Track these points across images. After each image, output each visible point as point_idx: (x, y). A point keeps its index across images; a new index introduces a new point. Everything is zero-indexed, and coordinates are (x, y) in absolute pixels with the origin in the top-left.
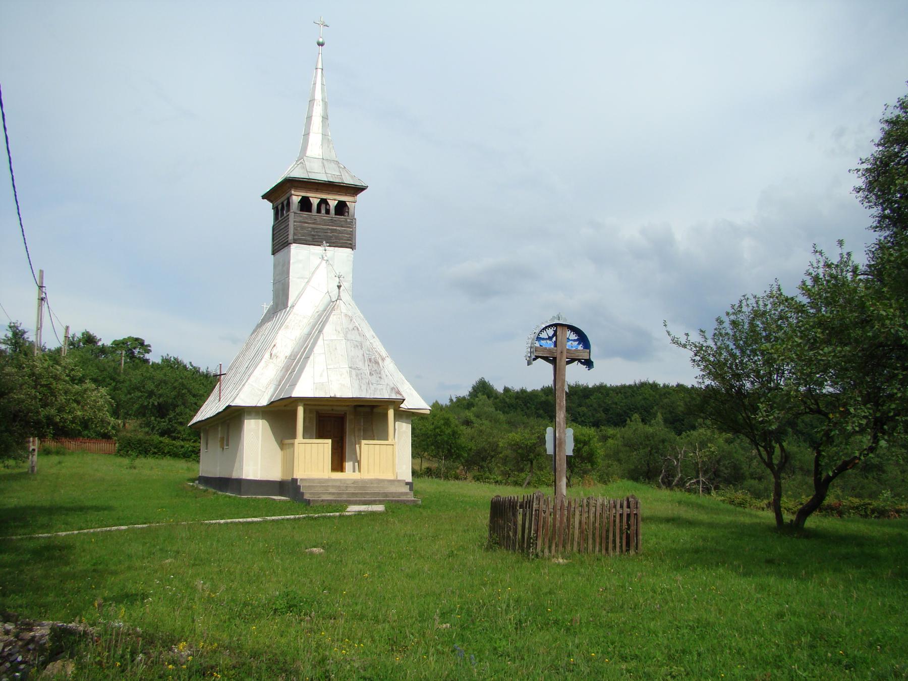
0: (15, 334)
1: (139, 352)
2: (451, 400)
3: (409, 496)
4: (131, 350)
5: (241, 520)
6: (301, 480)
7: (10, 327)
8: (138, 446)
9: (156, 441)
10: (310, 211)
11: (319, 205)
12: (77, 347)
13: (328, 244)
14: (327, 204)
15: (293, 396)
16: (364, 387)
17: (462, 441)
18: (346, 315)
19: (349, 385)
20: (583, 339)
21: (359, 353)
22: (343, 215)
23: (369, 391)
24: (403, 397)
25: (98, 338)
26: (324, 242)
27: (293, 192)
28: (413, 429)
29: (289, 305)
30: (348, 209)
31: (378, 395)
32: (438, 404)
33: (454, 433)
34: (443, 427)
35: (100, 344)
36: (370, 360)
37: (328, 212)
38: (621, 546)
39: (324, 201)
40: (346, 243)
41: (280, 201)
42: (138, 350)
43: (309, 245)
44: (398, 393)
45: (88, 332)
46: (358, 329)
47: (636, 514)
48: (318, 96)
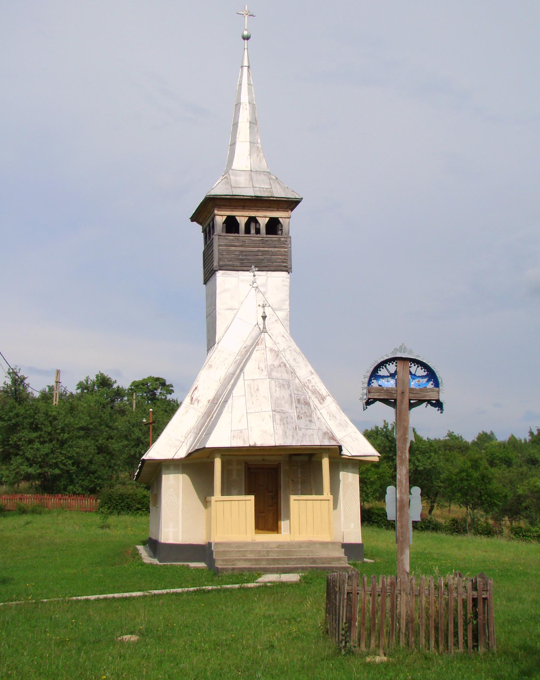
0: (15, 381)
1: (160, 393)
2: (531, 433)
3: (342, 562)
4: (152, 391)
5: (116, 595)
6: (216, 544)
7: (9, 374)
8: (120, 501)
9: (140, 496)
10: (238, 233)
11: (248, 225)
12: (91, 392)
13: (257, 269)
14: (257, 222)
15: (206, 446)
16: (289, 433)
17: (495, 486)
18: (271, 350)
19: (272, 431)
20: (431, 375)
21: (285, 394)
22: (276, 234)
23: (296, 438)
24: (338, 443)
25: (114, 380)
26: (253, 267)
27: (216, 212)
28: (363, 482)
29: (217, 340)
30: (282, 226)
31: (307, 442)
32: (515, 438)
33: (483, 477)
34: (470, 470)
35: (115, 386)
36: (299, 401)
37: (258, 231)
38: (466, 642)
39: (252, 220)
40: (280, 266)
41: (207, 223)
42: (159, 391)
43: (238, 271)
44: (333, 438)
45: (102, 374)
46: (285, 365)
47: (485, 599)
48: (245, 98)
